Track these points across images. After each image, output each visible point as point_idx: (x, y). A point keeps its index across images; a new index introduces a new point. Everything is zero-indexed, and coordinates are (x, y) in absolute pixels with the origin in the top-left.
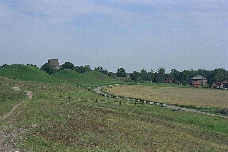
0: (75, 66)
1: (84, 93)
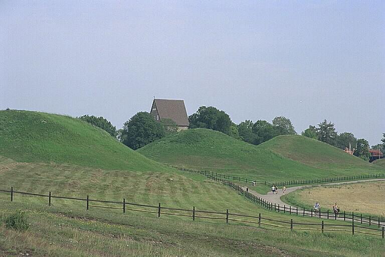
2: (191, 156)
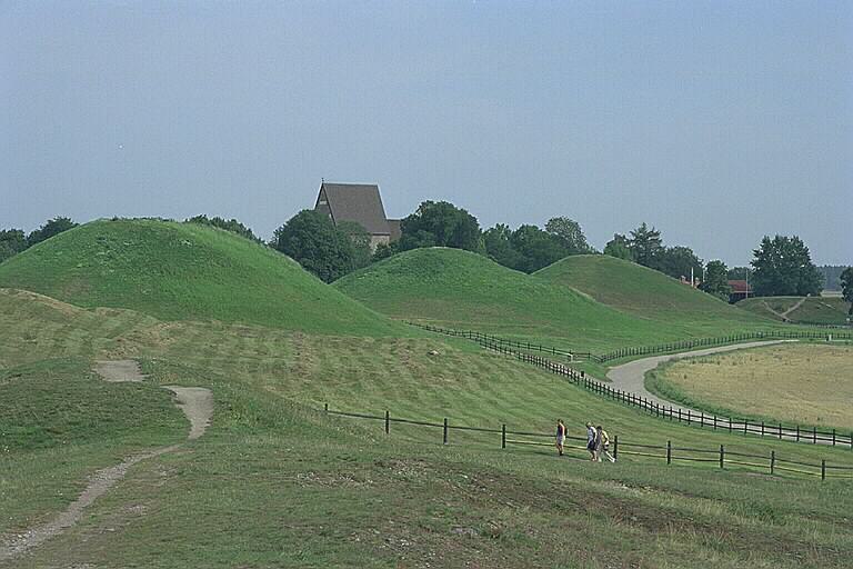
0: (484, 227)
1: (542, 395)
2: (429, 300)
